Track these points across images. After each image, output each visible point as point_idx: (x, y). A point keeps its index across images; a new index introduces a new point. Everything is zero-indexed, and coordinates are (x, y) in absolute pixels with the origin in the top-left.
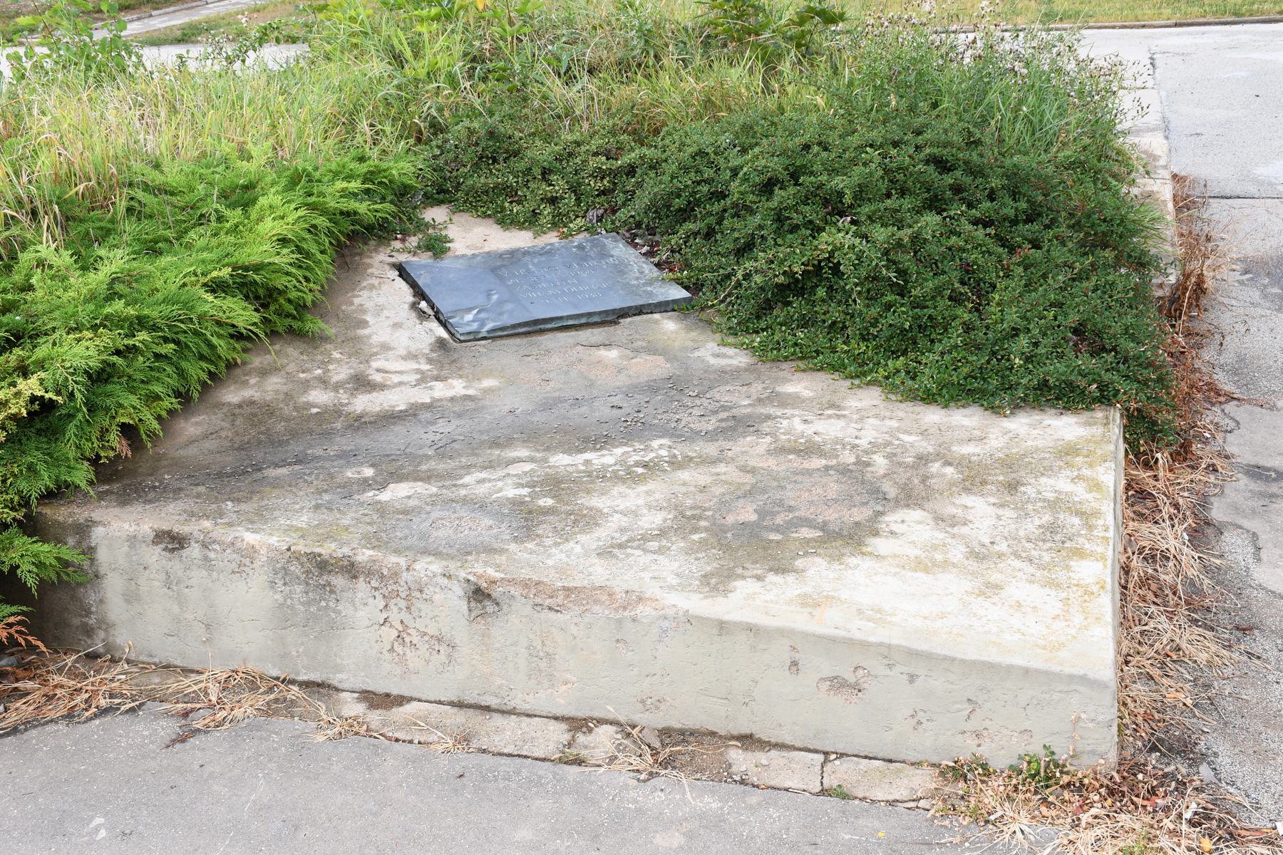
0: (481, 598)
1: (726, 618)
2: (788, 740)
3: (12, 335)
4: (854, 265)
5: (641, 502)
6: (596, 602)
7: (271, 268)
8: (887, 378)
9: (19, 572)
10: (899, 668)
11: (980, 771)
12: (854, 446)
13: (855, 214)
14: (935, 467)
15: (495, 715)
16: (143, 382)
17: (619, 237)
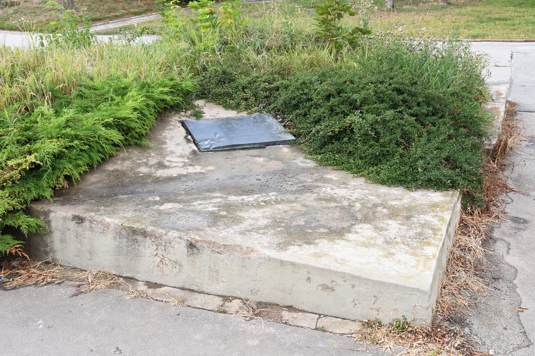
0: (192, 247)
1: (284, 259)
2: (306, 309)
3: (27, 139)
4: (359, 129)
5: (260, 215)
6: (236, 251)
7: (130, 119)
8: (368, 174)
9: (21, 228)
10: (348, 282)
11: (378, 324)
12: (349, 199)
13: (362, 109)
14: (379, 209)
15: (196, 293)
16: (75, 160)
17: (270, 115)
